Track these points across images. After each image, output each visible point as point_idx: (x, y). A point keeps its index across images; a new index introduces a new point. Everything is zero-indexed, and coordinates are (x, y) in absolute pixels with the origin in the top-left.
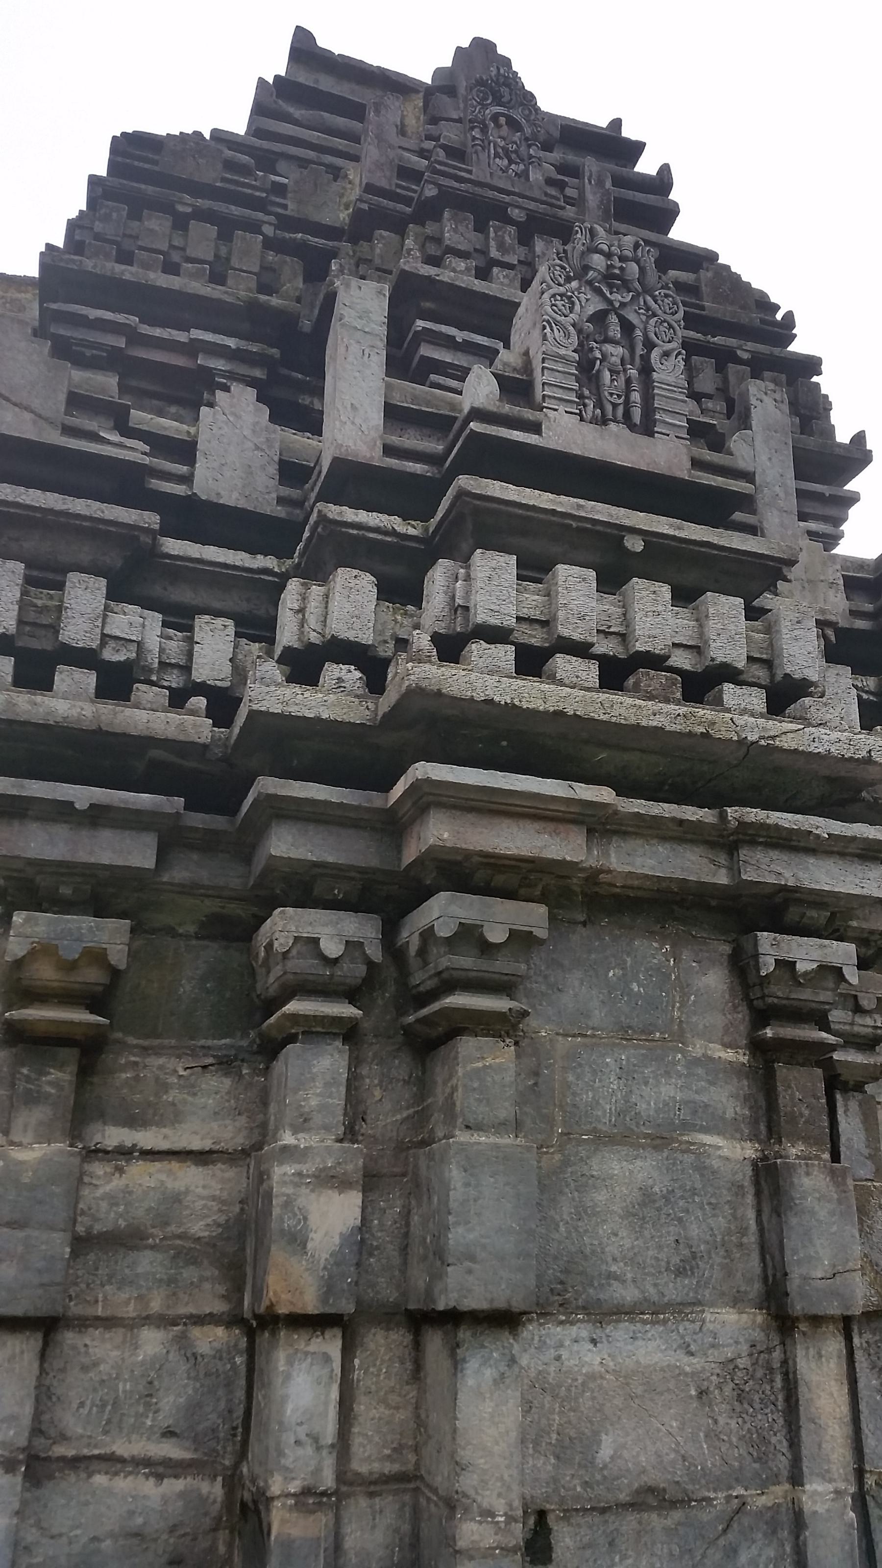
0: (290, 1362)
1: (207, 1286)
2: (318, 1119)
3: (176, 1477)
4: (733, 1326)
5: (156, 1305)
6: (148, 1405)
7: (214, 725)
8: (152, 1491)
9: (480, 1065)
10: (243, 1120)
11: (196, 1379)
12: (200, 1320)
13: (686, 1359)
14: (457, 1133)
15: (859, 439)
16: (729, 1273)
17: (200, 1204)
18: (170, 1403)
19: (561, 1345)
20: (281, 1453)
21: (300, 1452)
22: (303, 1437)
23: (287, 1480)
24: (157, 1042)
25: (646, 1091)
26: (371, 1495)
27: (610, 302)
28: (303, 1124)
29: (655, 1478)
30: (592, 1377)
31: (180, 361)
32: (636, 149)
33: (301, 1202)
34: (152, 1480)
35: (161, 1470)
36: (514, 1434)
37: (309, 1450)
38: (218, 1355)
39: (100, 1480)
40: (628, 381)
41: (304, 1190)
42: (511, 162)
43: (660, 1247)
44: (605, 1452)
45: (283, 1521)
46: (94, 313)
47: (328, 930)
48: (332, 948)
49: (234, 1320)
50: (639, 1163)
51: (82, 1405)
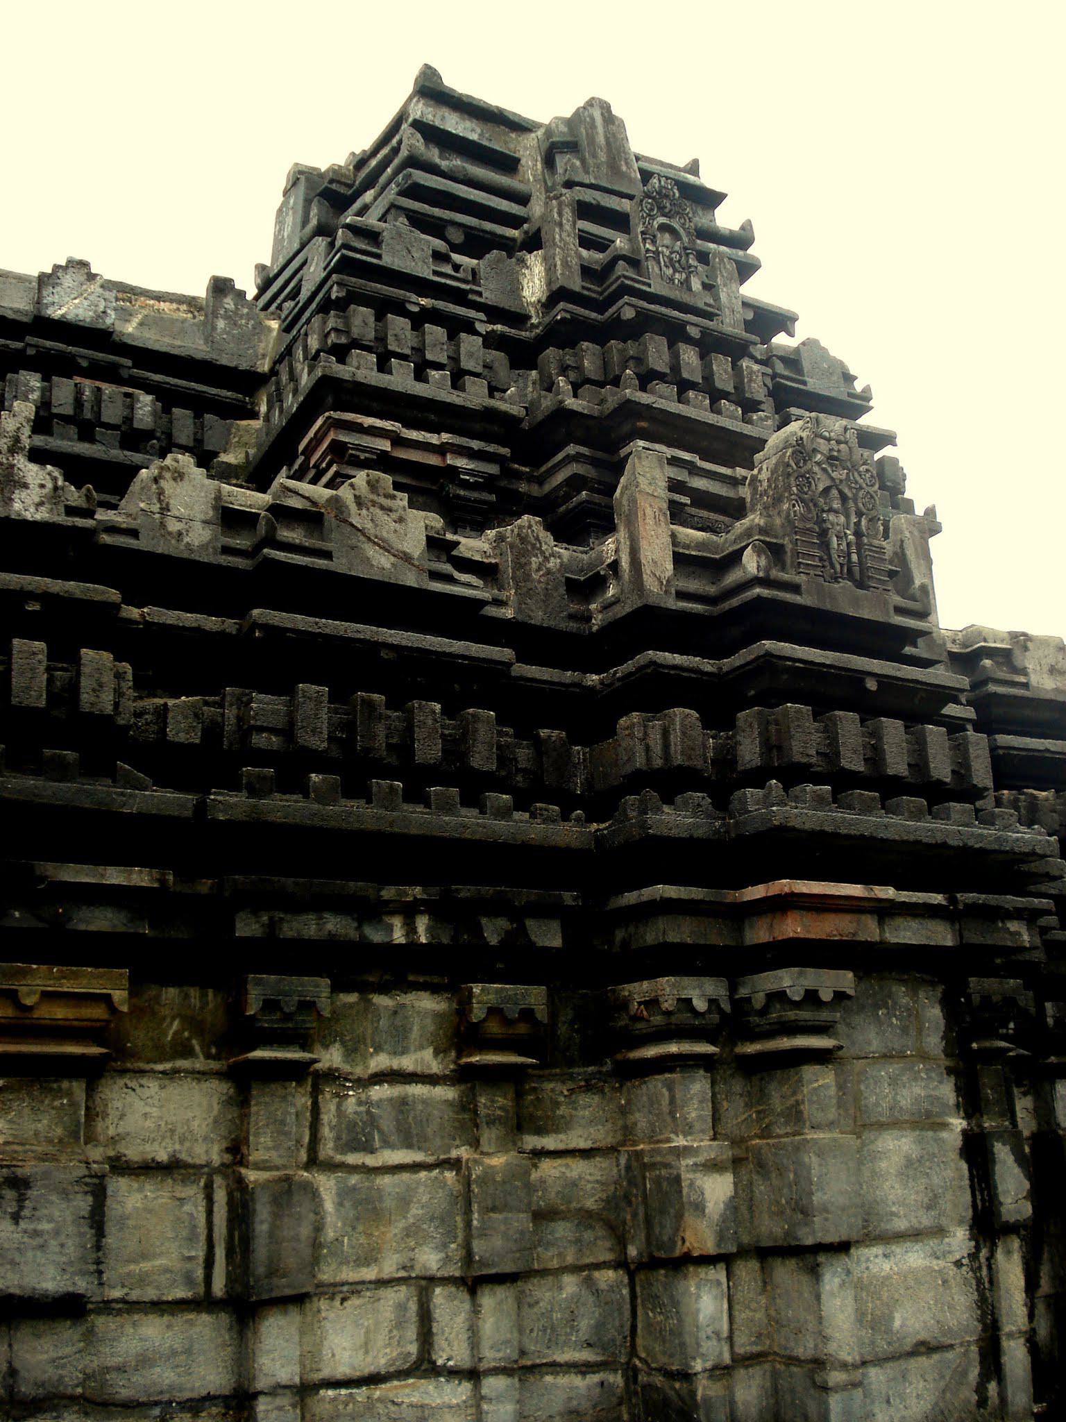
0: (698, 1287)
1: (600, 1243)
2: (697, 1126)
3: (594, 1373)
4: (959, 1239)
5: (570, 1259)
6: (572, 1327)
7: (115, 660)
8: (580, 1384)
9: (816, 1085)
10: (609, 1125)
11: (599, 1306)
12: (598, 1266)
13: (935, 1262)
14: (806, 1131)
15: (931, 512)
16: (955, 1206)
17: (589, 1186)
18: (585, 1325)
19: (868, 1260)
20: (698, 1345)
21: (710, 1343)
22: (710, 1333)
23: (704, 1361)
24: (547, 1072)
25: (905, 1092)
26: (747, 1367)
27: (833, 479)
28: (688, 1130)
29: (923, 1336)
30: (888, 1277)
31: (433, 460)
32: (712, 199)
33: (698, 1183)
34: (580, 1377)
35: (584, 1369)
36: (853, 1317)
37: (714, 1342)
38: (611, 1289)
39: (549, 1379)
40: (848, 545)
41: (698, 1175)
42: (675, 270)
43: (917, 1192)
44: (897, 1324)
45: (704, 1388)
46: (369, 421)
47: (697, 992)
48: (700, 1005)
49: (621, 1263)
50: (904, 1140)
51: (532, 1331)
